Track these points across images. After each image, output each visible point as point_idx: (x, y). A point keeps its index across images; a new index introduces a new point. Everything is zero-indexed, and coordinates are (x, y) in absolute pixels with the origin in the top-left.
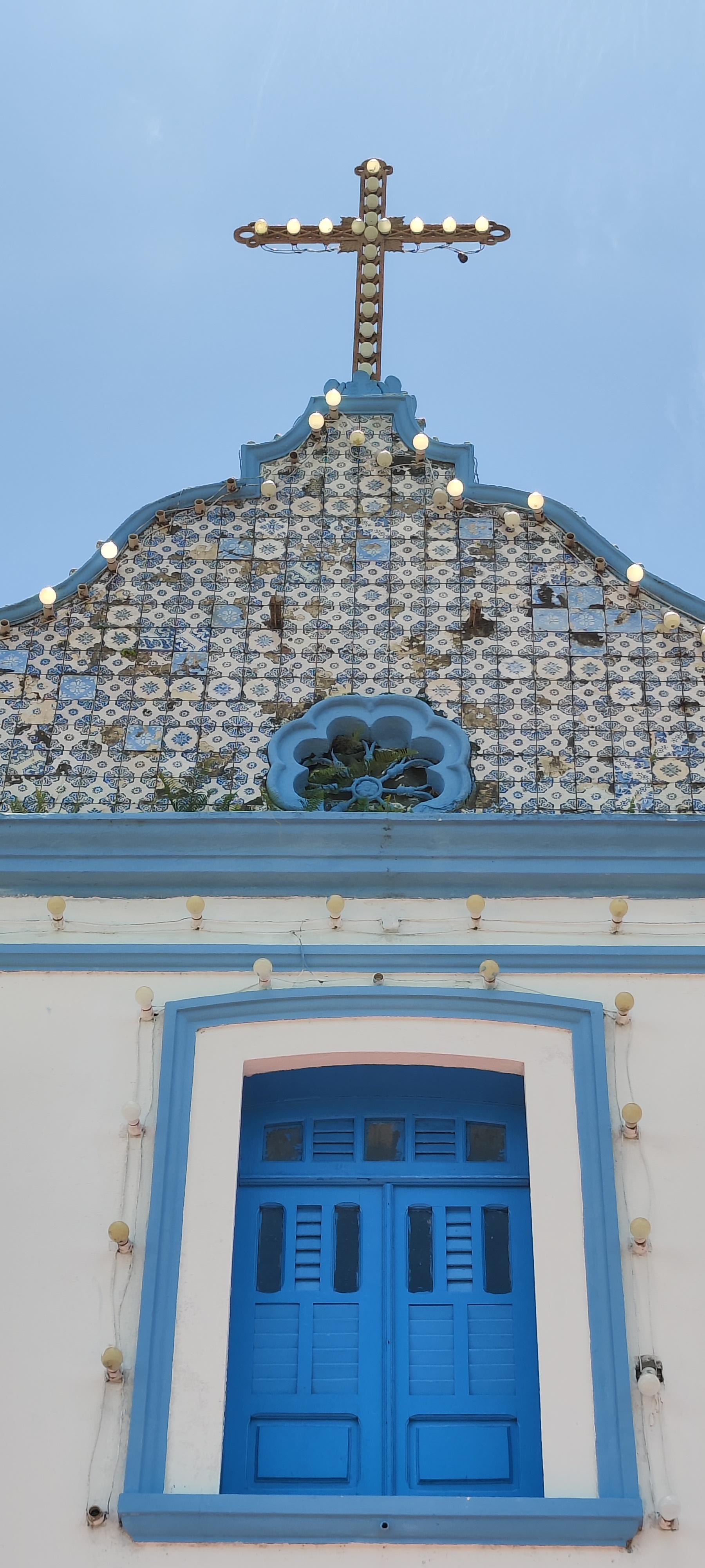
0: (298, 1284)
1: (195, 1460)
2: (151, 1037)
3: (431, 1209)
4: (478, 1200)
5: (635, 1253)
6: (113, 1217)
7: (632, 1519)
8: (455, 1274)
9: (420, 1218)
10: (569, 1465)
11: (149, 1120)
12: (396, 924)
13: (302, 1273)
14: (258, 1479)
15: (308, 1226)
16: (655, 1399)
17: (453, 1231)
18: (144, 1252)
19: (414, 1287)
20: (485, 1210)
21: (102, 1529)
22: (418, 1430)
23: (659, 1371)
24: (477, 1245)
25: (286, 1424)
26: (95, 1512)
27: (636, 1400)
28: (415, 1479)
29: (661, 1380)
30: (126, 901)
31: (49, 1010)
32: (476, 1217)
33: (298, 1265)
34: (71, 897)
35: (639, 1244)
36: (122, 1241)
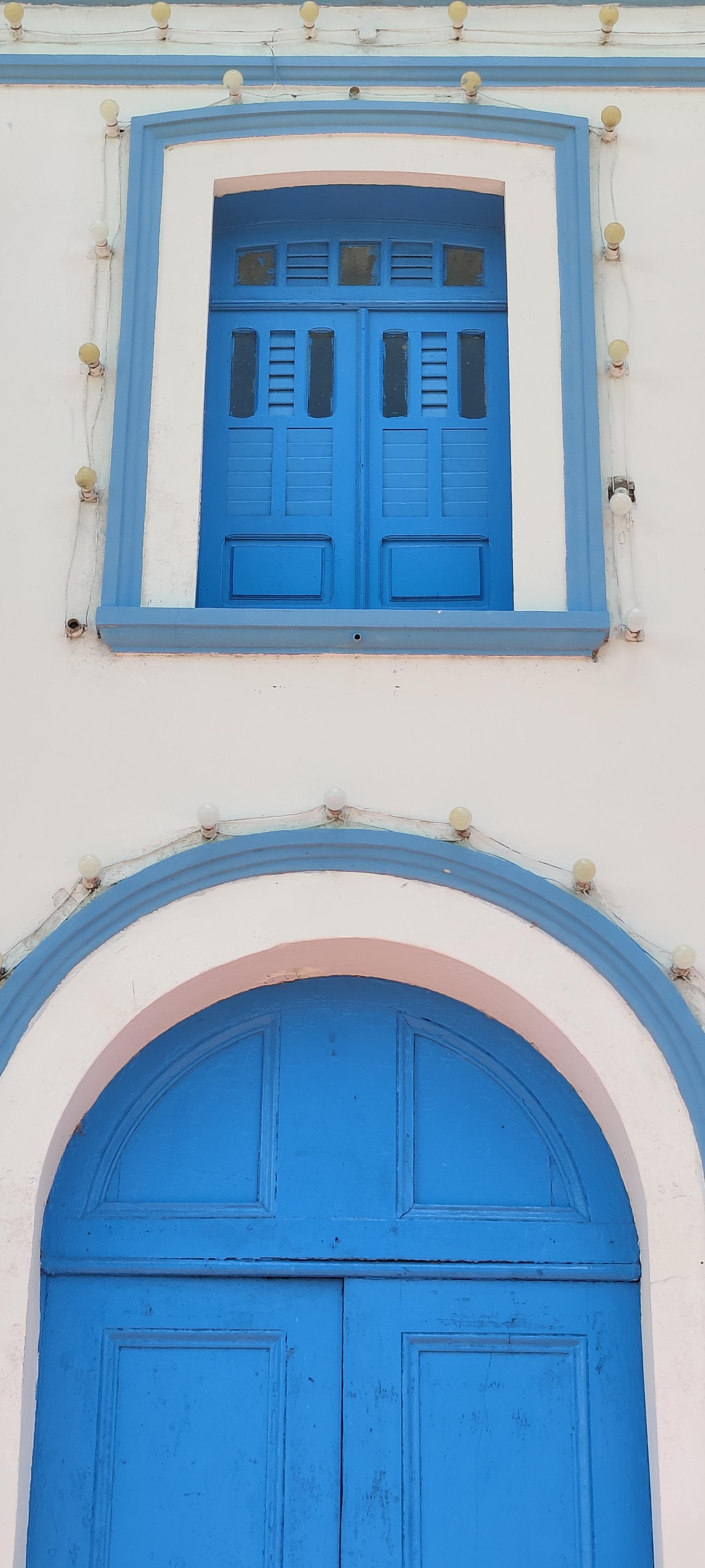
0: (272, 409)
1: (171, 574)
2: (118, 156)
3: (406, 334)
4: (454, 325)
5: (611, 376)
6: (82, 339)
7: (599, 630)
8: (430, 399)
9: (395, 343)
10: (539, 578)
11: (117, 240)
12: (373, 34)
13: (276, 398)
14: (234, 596)
15: (282, 352)
16: (627, 518)
17: (428, 357)
18: (115, 375)
19: (389, 411)
20: (462, 335)
21: (81, 640)
22: (391, 550)
23: (632, 491)
24: (452, 370)
25: (260, 544)
26: (73, 624)
27: (607, 519)
28: (387, 598)
29: (633, 500)
30: (88, 9)
31: (10, 125)
32: (452, 343)
33: (271, 391)
34: (29, 5)
35: (616, 367)
36: (93, 364)
